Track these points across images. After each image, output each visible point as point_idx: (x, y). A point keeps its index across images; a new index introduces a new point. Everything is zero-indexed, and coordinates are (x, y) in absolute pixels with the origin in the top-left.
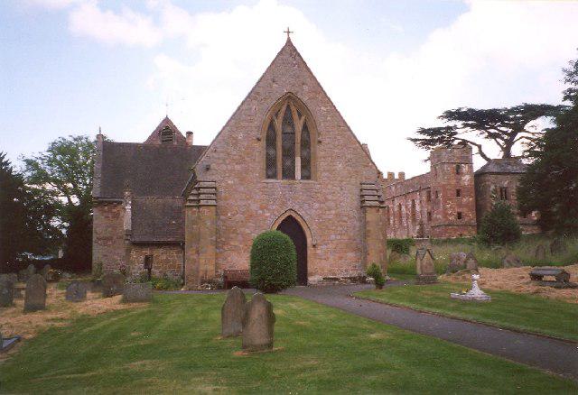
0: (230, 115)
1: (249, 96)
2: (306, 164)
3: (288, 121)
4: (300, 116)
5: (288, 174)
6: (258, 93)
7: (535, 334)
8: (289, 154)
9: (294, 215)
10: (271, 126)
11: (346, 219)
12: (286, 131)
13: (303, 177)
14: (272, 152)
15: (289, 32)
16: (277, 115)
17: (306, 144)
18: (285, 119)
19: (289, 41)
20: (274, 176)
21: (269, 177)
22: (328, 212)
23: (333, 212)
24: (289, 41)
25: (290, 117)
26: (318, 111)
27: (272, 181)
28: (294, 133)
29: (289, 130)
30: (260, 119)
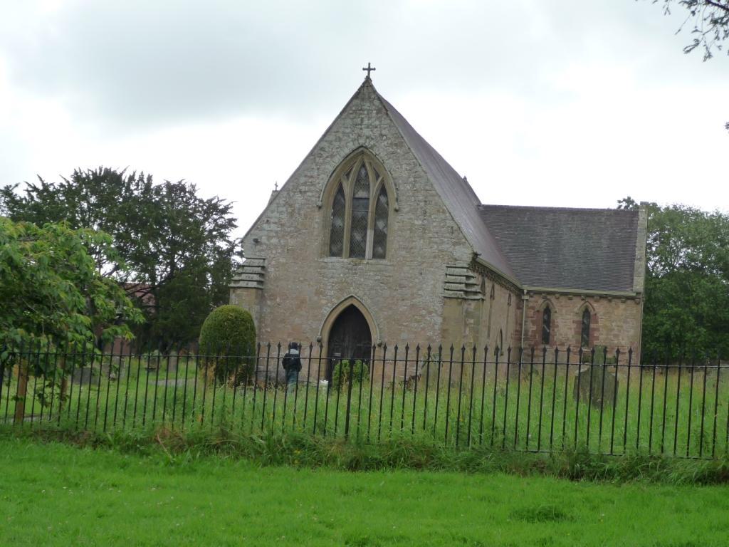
0: (402, 114)
1: (312, 153)
2: (380, 239)
3: (361, 182)
4: (378, 176)
5: (356, 251)
6: (322, 149)
7: (325, 322)
8: (359, 224)
9: (357, 304)
10: (340, 190)
11: (424, 312)
12: (357, 196)
13: (375, 256)
14: (339, 223)
15: (369, 69)
16: (348, 175)
17: (382, 213)
18: (358, 180)
19: (368, 80)
20: (337, 254)
21: (333, 254)
22: (400, 303)
23: (409, 303)
24: (368, 80)
25: (367, 172)
26: (397, 171)
27: (334, 259)
28: (368, 199)
29: (361, 194)
30: (322, 181)
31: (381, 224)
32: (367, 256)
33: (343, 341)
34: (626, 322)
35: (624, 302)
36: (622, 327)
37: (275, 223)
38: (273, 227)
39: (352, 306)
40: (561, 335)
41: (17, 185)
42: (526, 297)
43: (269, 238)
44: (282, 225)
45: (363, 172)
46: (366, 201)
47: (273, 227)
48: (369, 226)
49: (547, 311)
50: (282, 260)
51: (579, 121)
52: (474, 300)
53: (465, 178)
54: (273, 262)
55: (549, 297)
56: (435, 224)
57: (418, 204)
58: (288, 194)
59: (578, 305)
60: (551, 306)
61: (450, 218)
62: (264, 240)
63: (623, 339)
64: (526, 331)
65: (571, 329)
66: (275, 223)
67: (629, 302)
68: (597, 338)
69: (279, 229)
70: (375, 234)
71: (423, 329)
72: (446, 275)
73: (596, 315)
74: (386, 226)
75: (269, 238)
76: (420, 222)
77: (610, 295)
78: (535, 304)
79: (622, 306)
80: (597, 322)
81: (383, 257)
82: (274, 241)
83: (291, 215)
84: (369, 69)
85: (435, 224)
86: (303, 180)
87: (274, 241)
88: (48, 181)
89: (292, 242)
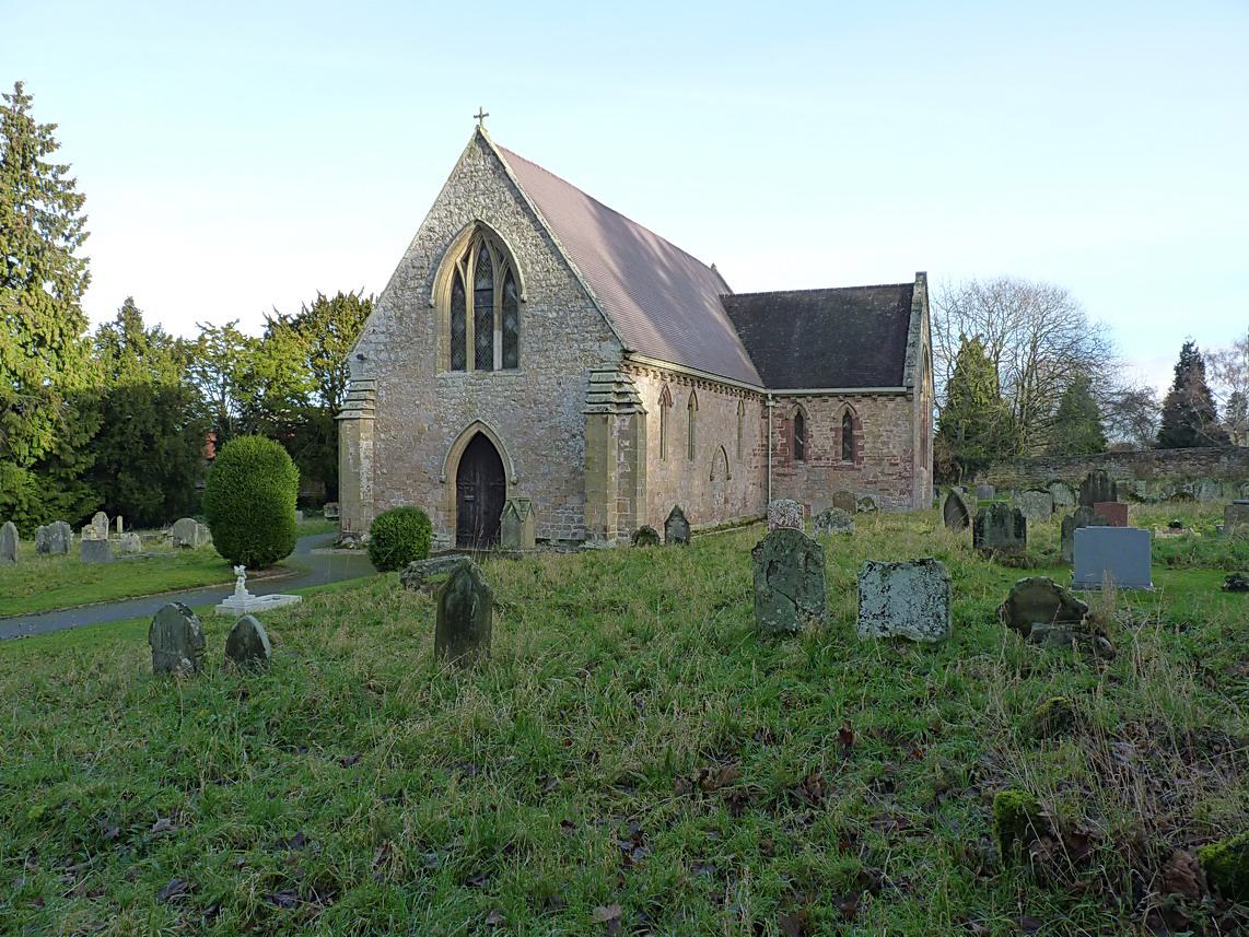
2: (511, 342)
5: (484, 362)
13: (505, 366)
15: (481, 117)
21: (455, 368)
23: (547, 424)
27: (456, 373)
28: (492, 290)
31: (510, 323)
32: (496, 367)
33: (475, 480)
34: (896, 425)
35: (892, 400)
36: (891, 431)
37: (383, 333)
38: (382, 338)
39: (479, 433)
40: (816, 446)
41: (238, 321)
42: (772, 403)
43: (378, 352)
44: (391, 334)
45: (484, 254)
46: (489, 293)
47: (382, 338)
48: (496, 326)
49: (800, 419)
50: (394, 380)
51: (1112, 238)
52: (628, 414)
53: (713, 266)
54: (384, 384)
55: (799, 400)
56: (573, 315)
57: (551, 291)
58: (395, 293)
59: (836, 409)
60: (802, 413)
61: (591, 305)
62: (372, 356)
63: (894, 447)
64: (774, 446)
65: (828, 438)
66: (383, 333)
67: (899, 399)
68: (862, 448)
69: (388, 340)
70: (504, 336)
71: (566, 458)
72: (590, 382)
73: (857, 418)
74: (517, 323)
75: (378, 352)
76: (555, 314)
77: (874, 393)
78: (783, 411)
79: (891, 405)
80: (861, 428)
81: (515, 365)
82: (383, 356)
83: (400, 319)
84: (481, 117)
85: (573, 315)
86: (412, 272)
87: (383, 356)
88: (284, 313)
89: (403, 355)
